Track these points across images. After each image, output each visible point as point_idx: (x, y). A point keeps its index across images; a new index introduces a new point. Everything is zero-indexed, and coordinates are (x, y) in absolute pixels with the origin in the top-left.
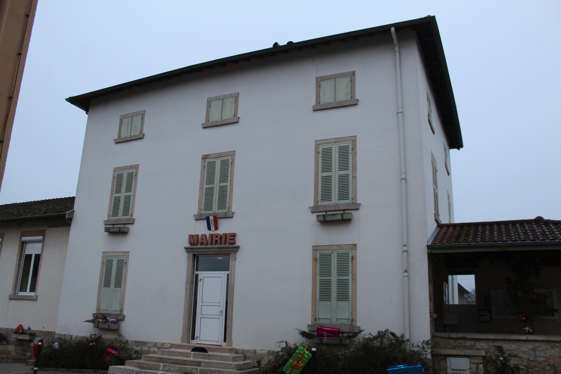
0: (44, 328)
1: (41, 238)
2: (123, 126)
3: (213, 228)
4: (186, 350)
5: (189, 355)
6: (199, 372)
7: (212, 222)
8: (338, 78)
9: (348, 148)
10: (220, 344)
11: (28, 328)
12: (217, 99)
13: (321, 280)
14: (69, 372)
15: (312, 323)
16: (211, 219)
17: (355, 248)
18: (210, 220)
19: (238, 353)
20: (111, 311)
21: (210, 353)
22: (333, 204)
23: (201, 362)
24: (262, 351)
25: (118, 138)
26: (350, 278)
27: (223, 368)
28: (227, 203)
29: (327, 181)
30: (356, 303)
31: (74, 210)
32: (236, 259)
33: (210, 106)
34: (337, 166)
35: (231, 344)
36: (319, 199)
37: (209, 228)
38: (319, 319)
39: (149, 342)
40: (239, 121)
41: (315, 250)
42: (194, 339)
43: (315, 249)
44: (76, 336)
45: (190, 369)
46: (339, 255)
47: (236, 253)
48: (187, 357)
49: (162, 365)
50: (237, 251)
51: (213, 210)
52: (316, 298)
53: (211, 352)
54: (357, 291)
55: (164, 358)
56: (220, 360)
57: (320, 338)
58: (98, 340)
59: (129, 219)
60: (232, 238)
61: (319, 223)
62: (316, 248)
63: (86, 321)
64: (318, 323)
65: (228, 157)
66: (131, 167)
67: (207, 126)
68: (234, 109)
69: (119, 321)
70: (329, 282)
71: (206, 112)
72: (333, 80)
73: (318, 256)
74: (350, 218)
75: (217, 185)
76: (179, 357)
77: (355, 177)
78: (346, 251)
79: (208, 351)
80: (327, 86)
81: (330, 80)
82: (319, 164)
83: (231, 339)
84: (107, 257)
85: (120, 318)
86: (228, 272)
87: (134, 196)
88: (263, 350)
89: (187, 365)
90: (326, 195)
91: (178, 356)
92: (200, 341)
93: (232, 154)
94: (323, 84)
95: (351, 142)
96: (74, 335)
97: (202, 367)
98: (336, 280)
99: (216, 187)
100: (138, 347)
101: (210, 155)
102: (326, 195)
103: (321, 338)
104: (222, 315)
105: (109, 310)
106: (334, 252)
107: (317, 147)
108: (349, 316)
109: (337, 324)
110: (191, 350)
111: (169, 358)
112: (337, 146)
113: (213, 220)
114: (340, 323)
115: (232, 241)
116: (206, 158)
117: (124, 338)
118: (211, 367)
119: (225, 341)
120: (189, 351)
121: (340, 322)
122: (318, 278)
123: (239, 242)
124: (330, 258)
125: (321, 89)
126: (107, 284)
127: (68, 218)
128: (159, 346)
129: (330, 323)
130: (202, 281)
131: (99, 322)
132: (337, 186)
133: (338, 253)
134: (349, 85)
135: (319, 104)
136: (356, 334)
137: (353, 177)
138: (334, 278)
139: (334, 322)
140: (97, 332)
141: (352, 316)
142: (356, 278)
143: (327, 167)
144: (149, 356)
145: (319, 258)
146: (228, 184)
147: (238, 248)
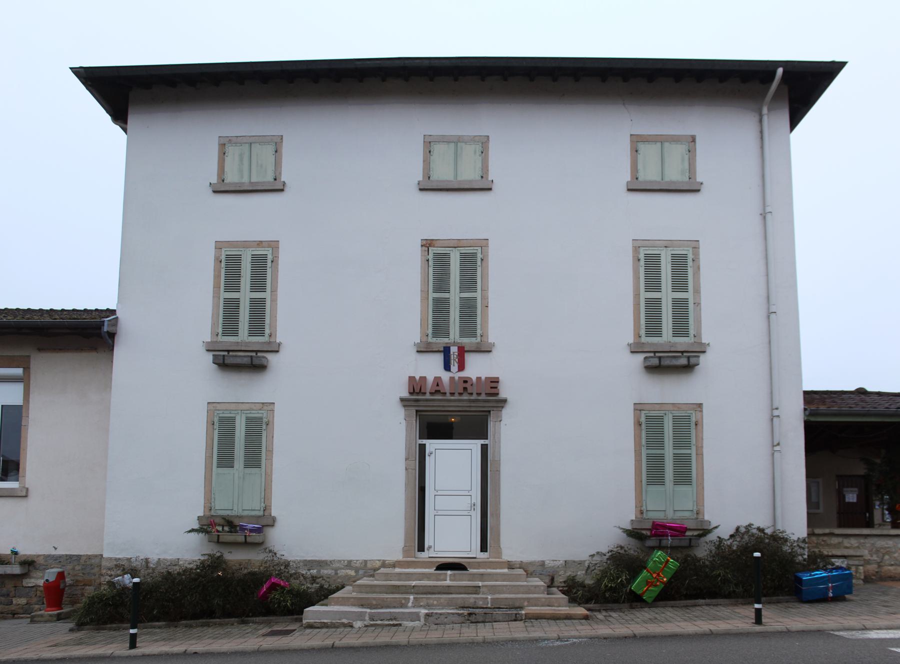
0: (56, 549)
1: (19, 371)
2: (228, 160)
3: (454, 367)
4: (425, 568)
5: (442, 577)
6: (490, 603)
7: (455, 356)
8: (667, 142)
9: (266, 258)
10: (475, 556)
11: (11, 550)
12: (445, 140)
13: (648, 455)
14: (176, 627)
15: (636, 518)
16: (454, 353)
17: (699, 409)
18: (452, 353)
19: (513, 567)
20: (240, 511)
21: (471, 571)
22: (665, 342)
23: (479, 587)
24: (555, 562)
25: (218, 183)
26: (693, 452)
27: (523, 594)
28: (479, 327)
29: (653, 307)
30: (703, 488)
31: (117, 318)
32: (500, 421)
33: (430, 152)
34: (458, 285)
35: (499, 553)
36: (643, 332)
37: (447, 367)
38: (647, 511)
39: (334, 561)
40: (285, 189)
41: (637, 410)
42: (424, 551)
43: (639, 408)
44: (159, 559)
45: (472, 601)
46: (676, 419)
47: (501, 411)
49: (412, 597)
51: (452, 336)
52: (641, 481)
53: (474, 568)
54: (705, 471)
55: (402, 586)
56: (504, 581)
57: (659, 538)
58: (214, 563)
59: (269, 343)
60: (494, 385)
61: (216, 366)
62: (639, 407)
63: (190, 531)
64: (647, 518)
65: (475, 248)
66: (260, 244)
67: (222, 189)
68: (479, 165)
69: (265, 529)
70: (661, 457)
71: (424, 161)
72: (659, 144)
73: (643, 419)
74: (265, 364)
75: (455, 296)
77: (697, 304)
78: (686, 413)
79: (467, 567)
80: (649, 152)
81: (654, 143)
82: (639, 278)
83: (500, 547)
84: (221, 412)
85: (266, 522)
86: (483, 442)
87: (274, 300)
88: (556, 561)
89: (451, 594)
90: (654, 328)
91: (420, 581)
92: (436, 552)
93: (483, 244)
94: (642, 147)
95: (691, 250)
96: (154, 557)
97: (483, 594)
98: (671, 455)
99: (453, 298)
100: (312, 571)
101: (462, 241)
102: (654, 328)
103: (661, 538)
104: (474, 509)
105: (235, 508)
106: (667, 414)
107: (636, 249)
108: (693, 506)
109: (676, 518)
110: (435, 569)
112: (669, 253)
113: (457, 354)
114: (680, 517)
115: (493, 391)
116: (430, 245)
117: (283, 557)
118: (499, 593)
119: (484, 548)
120: (432, 570)
121: (679, 515)
122: (644, 452)
123: (504, 392)
124: (661, 423)
125: (638, 155)
126: (225, 459)
127: (108, 332)
128: (358, 565)
129: (665, 517)
131: (218, 531)
132: (670, 315)
133: (674, 415)
134: (687, 157)
135: (635, 180)
136: (706, 532)
137: (694, 303)
138: (669, 452)
139: (670, 515)
140: (214, 550)
141: (697, 506)
142: (703, 452)
143: (653, 283)
144: (358, 585)
145: (644, 421)
146: (478, 295)
147: (505, 401)
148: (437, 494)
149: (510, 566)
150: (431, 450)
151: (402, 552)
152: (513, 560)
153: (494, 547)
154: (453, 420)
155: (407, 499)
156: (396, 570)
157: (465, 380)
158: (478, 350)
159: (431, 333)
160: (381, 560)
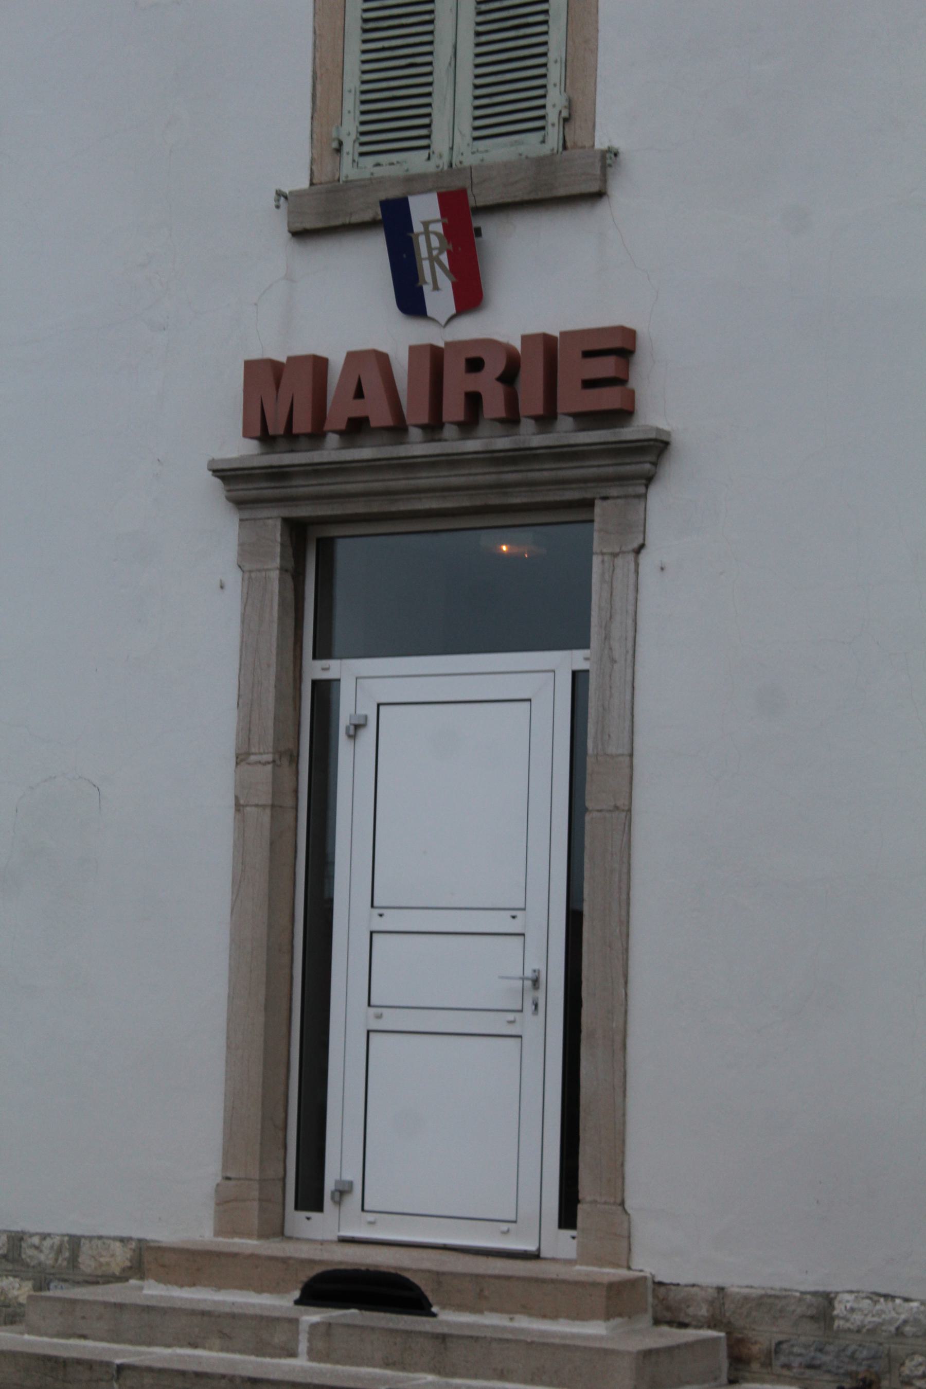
4: (260, 1290)
5: (279, 1338)
7: (435, 242)
10: (531, 1247)
16: (426, 224)
18: (417, 227)
24: (882, 1304)
28: (555, 73)
42: (319, 1208)
47: (644, 496)
48: (262, 1349)
50: (649, 480)
51: (440, 140)
53: (460, 1307)
55: (79, 1362)
60: (605, 367)
83: (622, 1204)
86: (577, 659)
91: (195, 1346)
92: (370, 1217)
110: (297, 1294)
111: (118, 1361)
113: (438, 228)
115: (607, 399)
128: (46, 1257)
148: (379, 924)
149: (668, 1308)
150: (361, 711)
151: (212, 1204)
152: (682, 1281)
153: (595, 1202)
154: (504, 548)
155: (236, 942)
156: (146, 1292)
157: (473, 354)
158: (540, 195)
159: (354, 135)
160: (130, 1239)
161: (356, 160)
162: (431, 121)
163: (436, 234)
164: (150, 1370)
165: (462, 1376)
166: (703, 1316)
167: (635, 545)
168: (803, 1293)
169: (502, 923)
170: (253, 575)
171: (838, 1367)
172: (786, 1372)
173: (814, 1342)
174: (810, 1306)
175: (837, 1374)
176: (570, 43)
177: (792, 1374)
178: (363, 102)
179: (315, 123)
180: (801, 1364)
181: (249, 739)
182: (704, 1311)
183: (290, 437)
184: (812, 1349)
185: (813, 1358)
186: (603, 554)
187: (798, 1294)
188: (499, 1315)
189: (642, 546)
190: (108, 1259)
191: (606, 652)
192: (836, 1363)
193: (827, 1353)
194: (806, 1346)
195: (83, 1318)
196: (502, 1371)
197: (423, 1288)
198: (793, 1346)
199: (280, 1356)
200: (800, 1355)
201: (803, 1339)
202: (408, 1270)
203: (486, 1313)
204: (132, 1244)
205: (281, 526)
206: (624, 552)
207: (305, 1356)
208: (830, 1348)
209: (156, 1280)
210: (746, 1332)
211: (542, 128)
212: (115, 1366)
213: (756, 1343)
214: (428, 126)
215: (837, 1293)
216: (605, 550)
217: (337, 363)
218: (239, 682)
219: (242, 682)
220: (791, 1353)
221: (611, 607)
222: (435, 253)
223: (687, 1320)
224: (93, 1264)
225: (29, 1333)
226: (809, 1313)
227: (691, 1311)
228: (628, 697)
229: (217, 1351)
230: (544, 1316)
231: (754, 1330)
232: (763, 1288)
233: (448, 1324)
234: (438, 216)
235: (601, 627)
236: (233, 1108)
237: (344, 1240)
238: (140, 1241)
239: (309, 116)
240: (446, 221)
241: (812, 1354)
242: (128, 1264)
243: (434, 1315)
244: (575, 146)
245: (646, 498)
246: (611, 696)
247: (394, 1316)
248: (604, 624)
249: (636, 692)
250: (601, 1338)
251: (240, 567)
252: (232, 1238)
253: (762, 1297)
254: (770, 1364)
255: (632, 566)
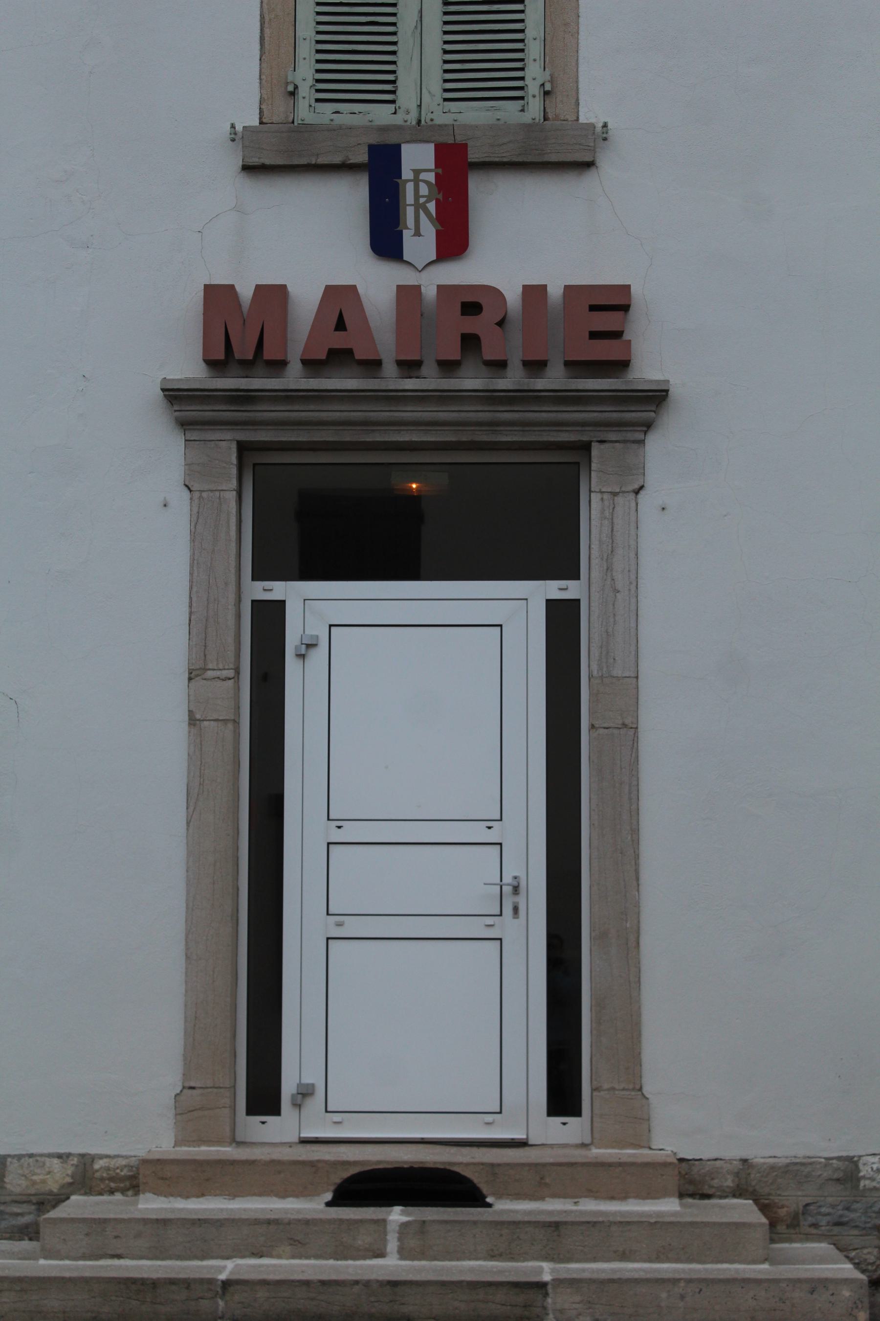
4: (283, 1195)
5: (363, 1239)
7: (424, 190)
10: (520, 1135)
16: (417, 172)
18: (407, 174)
19: (707, 1190)
23: (542, 1286)
28: (534, 50)
42: (274, 1109)
47: (642, 442)
48: (342, 1253)
50: (648, 426)
51: (407, 95)
53: (519, 1196)
55: (172, 1282)
60: (604, 321)
76: (265, 1261)
79: (485, 1189)
83: (640, 1089)
86: (554, 589)
92: (337, 1117)
104: (516, 910)
110: (329, 1196)
111: (223, 1277)
113: (431, 177)
130: (318, 657)
148: (337, 836)
149: (691, 1182)
151: (171, 1114)
154: (414, 486)
156: (140, 1206)
158: (529, 159)
159: (310, 82)
160: (69, 1155)
161: (313, 106)
162: (397, 77)
163: (426, 182)
164: (264, 1283)
165: (578, 1261)
166: (728, 1187)
167: (636, 486)
168: (826, 1159)
169: (479, 833)
170: (205, 495)
171: (866, 1223)
172: (814, 1231)
173: (841, 1201)
174: (837, 1169)
175: (864, 1229)
176: (549, 25)
177: (820, 1232)
178: (318, 51)
179: (264, 65)
180: (828, 1222)
181: (205, 656)
182: (729, 1182)
183: (247, 366)
184: (840, 1207)
185: (841, 1216)
186: (601, 492)
187: (823, 1160)
188: (562, 1200)
189: (642, 487)
190: (41, 1177)
191: (609, 582)
192: (863, 1219)
193: (855, 1211)
194: (833, 1206)
195: (116, 1237)
196: (624, 1253)
197: (476, 1181)
198: (820, 1207)
199: (364, 1258)
200: (829, 1214)
201: (830, 1200)
202: (455, 1164)
203: (547, 1199)
204: (73, 1160)
205: (586, 441)
206: (624, 492)
207: (396, 1256)
208: (856, 1206)
209: (154, 1194)
210: (771, 1197)
211: (522, 98)
212: (220, 1283)
213: (783, 1207)
214: (393, 82)
215: (860, 1157)
216: (603, 490)
217: (555, 291)
218: (191, 598)
219: (194, 599)
220: (819, 1213)
221: (613, 541)
222: (422, 200)
223: (710, 1192)
224: (24, 1183)
225: (45, 1258)
226: (835, 1176)
227: (715, 1183)
228: (633, 625)
229: (287, 1259)
230: (612, 1198)
231: (780, 1195)
232: (787, 1157)
233: (503, 1212)
234: (433, 167)
235: (602, 559)
236: (196, 1017)
237: (304, 1141)
238: (82, 1156)
239: (258, 57)
240: (440, 171)
241: (841, 1212)
242: (69, 1180)
243: (489, 1205)
244: (557, 118)
245: (644, 443)
246: (615, 623)
247: (378, 1209)
248: (605, 557)
249: (640, 619)
250: (675, 1214)
251: (186, 486)
252: (199, 1146)
253: (788, 1165)
254: (798, 1225)
255: (633, 504)
